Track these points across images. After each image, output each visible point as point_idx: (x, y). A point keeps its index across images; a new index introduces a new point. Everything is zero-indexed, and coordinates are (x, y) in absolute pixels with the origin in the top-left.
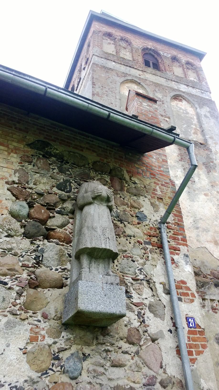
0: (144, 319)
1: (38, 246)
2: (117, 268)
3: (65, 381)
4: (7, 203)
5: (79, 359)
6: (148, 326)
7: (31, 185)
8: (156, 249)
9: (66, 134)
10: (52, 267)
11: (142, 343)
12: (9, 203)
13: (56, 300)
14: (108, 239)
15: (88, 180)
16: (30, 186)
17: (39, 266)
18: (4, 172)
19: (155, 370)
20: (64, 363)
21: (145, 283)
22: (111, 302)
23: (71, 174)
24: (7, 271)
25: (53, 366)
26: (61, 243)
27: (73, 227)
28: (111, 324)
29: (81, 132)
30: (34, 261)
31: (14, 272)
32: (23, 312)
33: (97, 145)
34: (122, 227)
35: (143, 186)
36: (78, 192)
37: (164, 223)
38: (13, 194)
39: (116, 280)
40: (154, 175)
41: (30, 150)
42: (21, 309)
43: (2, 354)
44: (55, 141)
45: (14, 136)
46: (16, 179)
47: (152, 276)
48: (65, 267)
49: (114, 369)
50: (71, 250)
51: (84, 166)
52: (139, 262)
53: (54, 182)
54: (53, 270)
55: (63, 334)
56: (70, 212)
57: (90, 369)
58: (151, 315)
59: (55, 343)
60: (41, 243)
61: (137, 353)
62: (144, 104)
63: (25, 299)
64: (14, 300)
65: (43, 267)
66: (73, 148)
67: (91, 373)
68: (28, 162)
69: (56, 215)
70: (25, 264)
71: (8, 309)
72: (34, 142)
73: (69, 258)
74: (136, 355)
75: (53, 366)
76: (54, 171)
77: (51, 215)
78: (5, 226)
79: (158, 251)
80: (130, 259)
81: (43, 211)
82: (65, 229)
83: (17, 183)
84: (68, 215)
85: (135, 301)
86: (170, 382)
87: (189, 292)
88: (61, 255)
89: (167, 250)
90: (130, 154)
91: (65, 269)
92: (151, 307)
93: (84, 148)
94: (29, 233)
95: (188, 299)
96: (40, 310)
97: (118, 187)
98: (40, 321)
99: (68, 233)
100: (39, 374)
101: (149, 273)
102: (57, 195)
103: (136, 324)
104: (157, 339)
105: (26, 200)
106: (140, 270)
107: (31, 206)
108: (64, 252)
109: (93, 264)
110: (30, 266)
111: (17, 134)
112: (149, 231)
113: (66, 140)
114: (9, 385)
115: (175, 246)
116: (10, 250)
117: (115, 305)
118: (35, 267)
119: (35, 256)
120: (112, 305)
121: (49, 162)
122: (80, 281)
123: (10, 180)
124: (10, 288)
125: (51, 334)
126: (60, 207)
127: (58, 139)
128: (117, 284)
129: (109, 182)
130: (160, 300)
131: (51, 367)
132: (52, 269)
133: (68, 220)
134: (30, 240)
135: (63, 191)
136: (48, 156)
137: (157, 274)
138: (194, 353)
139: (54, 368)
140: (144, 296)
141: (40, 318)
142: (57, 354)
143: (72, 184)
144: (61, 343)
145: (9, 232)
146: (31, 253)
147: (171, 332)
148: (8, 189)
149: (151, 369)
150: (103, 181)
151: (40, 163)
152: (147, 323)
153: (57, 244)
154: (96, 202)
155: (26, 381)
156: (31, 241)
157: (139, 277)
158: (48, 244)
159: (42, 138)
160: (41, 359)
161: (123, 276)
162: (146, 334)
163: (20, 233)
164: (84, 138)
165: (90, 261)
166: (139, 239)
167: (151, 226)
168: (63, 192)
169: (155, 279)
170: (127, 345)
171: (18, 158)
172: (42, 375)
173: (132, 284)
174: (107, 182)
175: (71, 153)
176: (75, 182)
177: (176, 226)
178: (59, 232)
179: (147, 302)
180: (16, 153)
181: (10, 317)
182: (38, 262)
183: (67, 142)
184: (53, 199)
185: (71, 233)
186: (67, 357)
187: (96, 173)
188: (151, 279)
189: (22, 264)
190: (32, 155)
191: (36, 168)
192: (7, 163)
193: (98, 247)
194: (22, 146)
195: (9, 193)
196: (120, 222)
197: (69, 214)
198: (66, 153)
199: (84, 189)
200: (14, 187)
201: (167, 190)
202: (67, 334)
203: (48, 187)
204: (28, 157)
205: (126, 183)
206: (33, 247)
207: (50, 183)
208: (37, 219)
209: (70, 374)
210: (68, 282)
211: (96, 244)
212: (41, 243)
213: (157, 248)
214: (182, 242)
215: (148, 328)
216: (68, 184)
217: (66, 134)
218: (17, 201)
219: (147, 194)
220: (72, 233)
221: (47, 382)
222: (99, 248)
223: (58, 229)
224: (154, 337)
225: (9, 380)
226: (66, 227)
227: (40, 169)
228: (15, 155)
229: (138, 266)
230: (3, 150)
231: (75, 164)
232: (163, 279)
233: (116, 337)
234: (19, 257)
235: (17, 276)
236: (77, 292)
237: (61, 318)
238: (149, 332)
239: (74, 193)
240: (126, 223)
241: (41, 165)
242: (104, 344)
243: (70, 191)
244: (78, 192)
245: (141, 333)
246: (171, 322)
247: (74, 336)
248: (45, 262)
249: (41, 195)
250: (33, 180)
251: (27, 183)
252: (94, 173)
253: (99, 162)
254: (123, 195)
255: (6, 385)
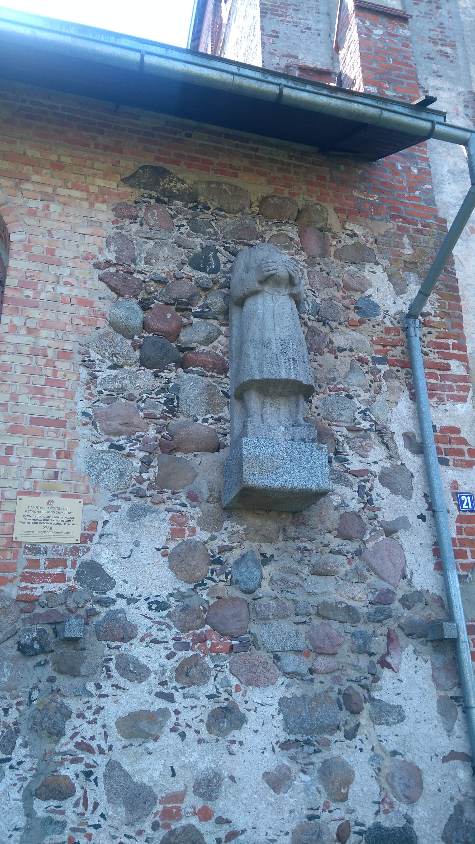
0: (371, 499)
1: (169, 382)
2: (317, 411)
3: (234, 596)
4: (102, 307)
5: (256, 562)
6: (379, 509)
7: (142, 266)
8: (398, 371)
9: (200, 142)
10: (198, 417)
11: (367, 537)
12: (106, 303)
13: (209, 471)
14: (291, 362)
15: (252, 242)
16: (139, 267)
17: (174, 415)
18: (88, 244)
19: (392, 581)
20: (230, 569)
21: (373, 435)
22: (302, 470)
23: (216, 233)
24: (120, 427)
25: (212, 573)
26: (209, 374)
27: (228, 342)
28: (308, 506)
29: (231, 131)
30: (165, 408)
31: (133, 428)
32: (155, 492)
33: (267, 156)
34: (326, 334)
35: (371, 240)
36: (231, 271)
37: (415, 317)
38: (110, 286)
39: (310, 434)
40: (398, 210)
41: (130, 190)
42: (151, 487)
43: (129, 556)
44: (178, 163)
45: (97, 165)
46: (112, 257)
47: (388, 422)
48: (220, 415)
49: (317, 578)
50: (227, 383)
51: (242, 211)
52: (360, 399)
53: (183, 254)
54: (200, 422)
55: (226, 524)
56: (220, 313)
57: (275, 578)
58: (385, 492)
59: (213, 538)
60: (173, 374)
61: (359, 553)
62: (375, 32)
63: (156, 471)
64: (138, 474)
65: (182, 417)
66: (217, 171)
67: (277, 584)
68: (131, 217)
69: (195, 320)
70: (150, 414)
71: (131, 488)
72: (136, 172)
73: (226, 399)
74: (356, 557)
75: (212, 573)
76: (183, 230)
77: (185, 320)
78: (105, 349)
79: (402, 374)
80: (344, 394)
81: (169, 316)
82: (214, 347)
83: (115, 265)
84: (216, 319)
85: (353, 467)
86: (420, 601)
87: (465, 448)
88: (209, 392)
89: (421, 372)
90: (342, 167)
91: (221, 418)
92: (385, 478)
93: (239, 169)
94: (149, 359)
95: (462, 461)
96: (183, 488)
97: (315, 249)
98: (185, 505)
99: (220, 354)
100: (192, 586)
101: (382, 418)
102: (191, 280)
103: (355, 505)
104: (396, 531)
105: (136, 297)
106: (363, 412)
107: (145, 306)
108: (216, 388)
109: (268, 407)
110: (158, 416)
111: (101, 159)
112: (383, 335)
113: (201, 157)
114: (146, 600)
115: (438, 361)
116: (120, 391)
117: (309, 476)
118: (166, 418)
119: (164, 399)
120: (305, 476)
121: (170, 212)
122: (245, 439)
123: (101, 259)
124: (129, 455)
125: (203, 523)
126: (201, 303)
127: (182, 156)
128: (313, 441)
129: (297, 239)
130: (402, 464)
131: (209, 575)
132: (197, 420)
133: (218, 329)
134: (152, 371)
135: (203, 270)
136: (166, 200)
137: (400, 417)
138: (469, 554)
139: (214, 577)
140: (371, 459)
141: (184, 500)
142: (218, 556)
143: (219, 254)
144: (223, 539)
145: (115, 359)
146: (157, 395)
147: (424, 520)
148: (100, 279)
149: (384, 580)
150: (282, 239)
151: (154, 215)
152: (376, 504)
153: (202, 376)
154: (266, 289)
155: (171, 595)
156: (154, 372)
157: (361, 426)
158: (186, 376)
159: (149, 161)
160: (191, 564)
161: (329, 425)
162: (376, 522)
163: (134, 360)
164: (237, 146)
165: (263, 403)
166: (361, 355)
167: (389, 324)
168: (203, 274)
169: (393, 427)
170: (339, 541)
171: (110, 212)
172: (196, 586)
173: (347, 437)
174: (291, 239)
175: (212, 186)
176: (226, 249)
177: (444, 320)
178: (203, 353)
179: (376, 469)
180: (104, 202)
181: (136, 500)
182: (172, 408)
183: (204, 161)
184: (183, 290)
185: (225, 354)
186: (236, 559)
187: (267, 224)
188: (385, 427)
189: (145, 414)
190: (136, 202)
191: (145, 228)
192: (91, 226)
193: (274, 377)
194: (114, 185)
195: (103, 286)
196: (321, 323)
197: (219, 317)
198: (202, 187)
199: (243, 264)
200: (111, 273)
201: (426, 243)
202: (233, 524)
203: (173, 267)
204: (128, 207)
205: (334, 238)
206: (159, 383)
207: (177, 257)
208: (160, 331)
209: (242, 585)
210: (228, 440)
211: (269, 371)
212: (172, 374)
213: (399, 368)
214: (456, 352)
215: (377, 513)
216: (211, 254)
217: (200, 142)
218: (120, 299)
219: (381, 255)
220: (227, 352)
221: (205, 596)
222: (276, 380)
223: (202, 348)
224: (390, 528)
225: (144, 593)
226: (215, 343)
227: (154, 231)
228: (104, 207)
229: (359, 405)
230: (79, 199)
231: (221, 210)
232: (410, 426)
233: (319, 528)
234: (137, 402)
235: (137, 434)
236: (241, 456)
237: (219, 499)
238: (380, 519)
239: (225, 272)
240: (334, 324)
241: (155, 220)
242: (298, 539)
243: (216, 270)
244: (231, 271)
245: (366, 521)
246: (424, 501)
247: (245, 527)
248: (183, 408)
249: (161, 282)
250: (144, 256)
251: (134, 261)
252: (264, 223)
253: (273, 197)
254: (327, 265)
255: (142, 599)
